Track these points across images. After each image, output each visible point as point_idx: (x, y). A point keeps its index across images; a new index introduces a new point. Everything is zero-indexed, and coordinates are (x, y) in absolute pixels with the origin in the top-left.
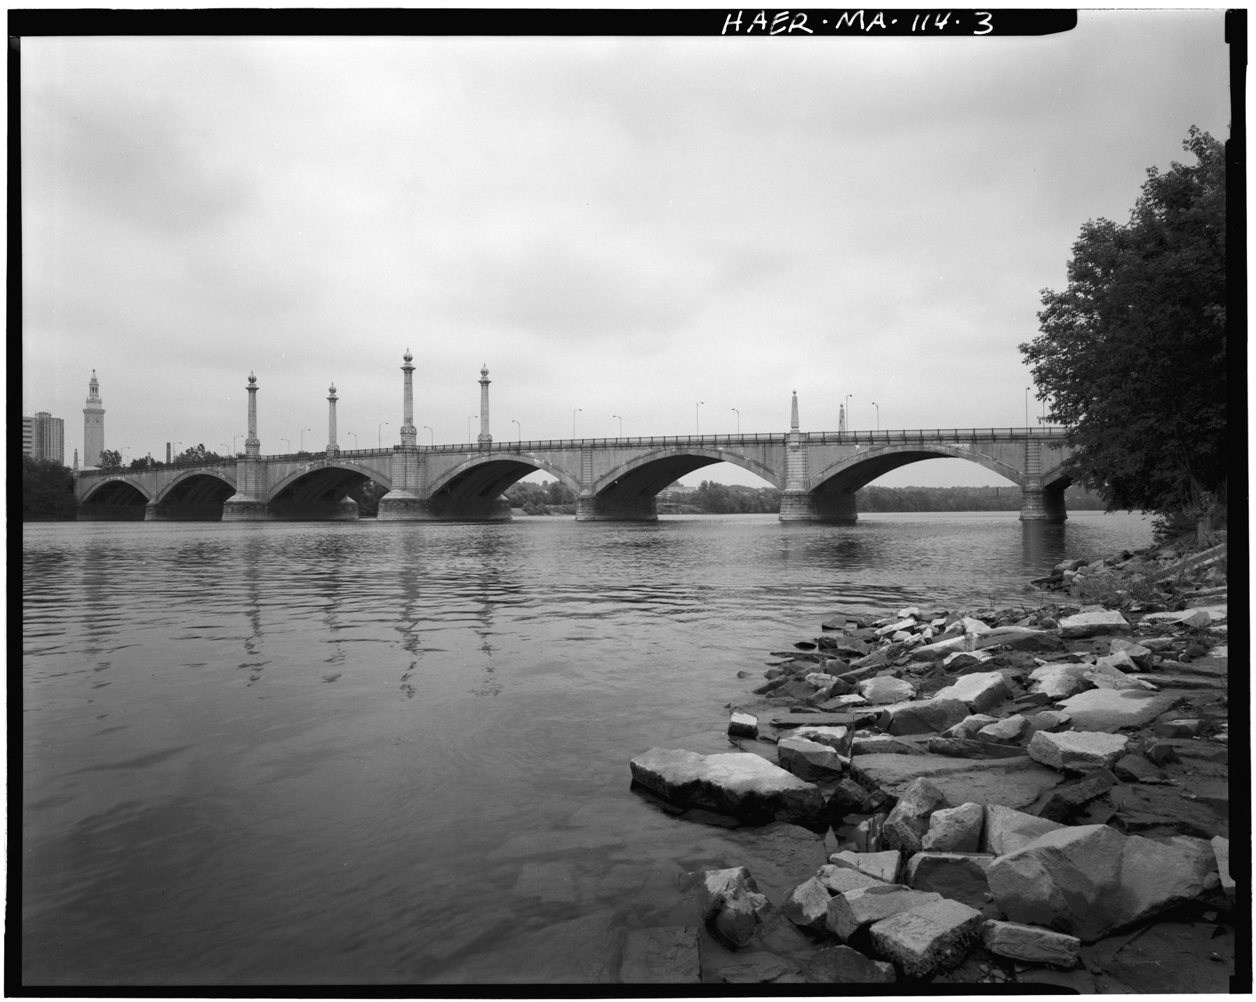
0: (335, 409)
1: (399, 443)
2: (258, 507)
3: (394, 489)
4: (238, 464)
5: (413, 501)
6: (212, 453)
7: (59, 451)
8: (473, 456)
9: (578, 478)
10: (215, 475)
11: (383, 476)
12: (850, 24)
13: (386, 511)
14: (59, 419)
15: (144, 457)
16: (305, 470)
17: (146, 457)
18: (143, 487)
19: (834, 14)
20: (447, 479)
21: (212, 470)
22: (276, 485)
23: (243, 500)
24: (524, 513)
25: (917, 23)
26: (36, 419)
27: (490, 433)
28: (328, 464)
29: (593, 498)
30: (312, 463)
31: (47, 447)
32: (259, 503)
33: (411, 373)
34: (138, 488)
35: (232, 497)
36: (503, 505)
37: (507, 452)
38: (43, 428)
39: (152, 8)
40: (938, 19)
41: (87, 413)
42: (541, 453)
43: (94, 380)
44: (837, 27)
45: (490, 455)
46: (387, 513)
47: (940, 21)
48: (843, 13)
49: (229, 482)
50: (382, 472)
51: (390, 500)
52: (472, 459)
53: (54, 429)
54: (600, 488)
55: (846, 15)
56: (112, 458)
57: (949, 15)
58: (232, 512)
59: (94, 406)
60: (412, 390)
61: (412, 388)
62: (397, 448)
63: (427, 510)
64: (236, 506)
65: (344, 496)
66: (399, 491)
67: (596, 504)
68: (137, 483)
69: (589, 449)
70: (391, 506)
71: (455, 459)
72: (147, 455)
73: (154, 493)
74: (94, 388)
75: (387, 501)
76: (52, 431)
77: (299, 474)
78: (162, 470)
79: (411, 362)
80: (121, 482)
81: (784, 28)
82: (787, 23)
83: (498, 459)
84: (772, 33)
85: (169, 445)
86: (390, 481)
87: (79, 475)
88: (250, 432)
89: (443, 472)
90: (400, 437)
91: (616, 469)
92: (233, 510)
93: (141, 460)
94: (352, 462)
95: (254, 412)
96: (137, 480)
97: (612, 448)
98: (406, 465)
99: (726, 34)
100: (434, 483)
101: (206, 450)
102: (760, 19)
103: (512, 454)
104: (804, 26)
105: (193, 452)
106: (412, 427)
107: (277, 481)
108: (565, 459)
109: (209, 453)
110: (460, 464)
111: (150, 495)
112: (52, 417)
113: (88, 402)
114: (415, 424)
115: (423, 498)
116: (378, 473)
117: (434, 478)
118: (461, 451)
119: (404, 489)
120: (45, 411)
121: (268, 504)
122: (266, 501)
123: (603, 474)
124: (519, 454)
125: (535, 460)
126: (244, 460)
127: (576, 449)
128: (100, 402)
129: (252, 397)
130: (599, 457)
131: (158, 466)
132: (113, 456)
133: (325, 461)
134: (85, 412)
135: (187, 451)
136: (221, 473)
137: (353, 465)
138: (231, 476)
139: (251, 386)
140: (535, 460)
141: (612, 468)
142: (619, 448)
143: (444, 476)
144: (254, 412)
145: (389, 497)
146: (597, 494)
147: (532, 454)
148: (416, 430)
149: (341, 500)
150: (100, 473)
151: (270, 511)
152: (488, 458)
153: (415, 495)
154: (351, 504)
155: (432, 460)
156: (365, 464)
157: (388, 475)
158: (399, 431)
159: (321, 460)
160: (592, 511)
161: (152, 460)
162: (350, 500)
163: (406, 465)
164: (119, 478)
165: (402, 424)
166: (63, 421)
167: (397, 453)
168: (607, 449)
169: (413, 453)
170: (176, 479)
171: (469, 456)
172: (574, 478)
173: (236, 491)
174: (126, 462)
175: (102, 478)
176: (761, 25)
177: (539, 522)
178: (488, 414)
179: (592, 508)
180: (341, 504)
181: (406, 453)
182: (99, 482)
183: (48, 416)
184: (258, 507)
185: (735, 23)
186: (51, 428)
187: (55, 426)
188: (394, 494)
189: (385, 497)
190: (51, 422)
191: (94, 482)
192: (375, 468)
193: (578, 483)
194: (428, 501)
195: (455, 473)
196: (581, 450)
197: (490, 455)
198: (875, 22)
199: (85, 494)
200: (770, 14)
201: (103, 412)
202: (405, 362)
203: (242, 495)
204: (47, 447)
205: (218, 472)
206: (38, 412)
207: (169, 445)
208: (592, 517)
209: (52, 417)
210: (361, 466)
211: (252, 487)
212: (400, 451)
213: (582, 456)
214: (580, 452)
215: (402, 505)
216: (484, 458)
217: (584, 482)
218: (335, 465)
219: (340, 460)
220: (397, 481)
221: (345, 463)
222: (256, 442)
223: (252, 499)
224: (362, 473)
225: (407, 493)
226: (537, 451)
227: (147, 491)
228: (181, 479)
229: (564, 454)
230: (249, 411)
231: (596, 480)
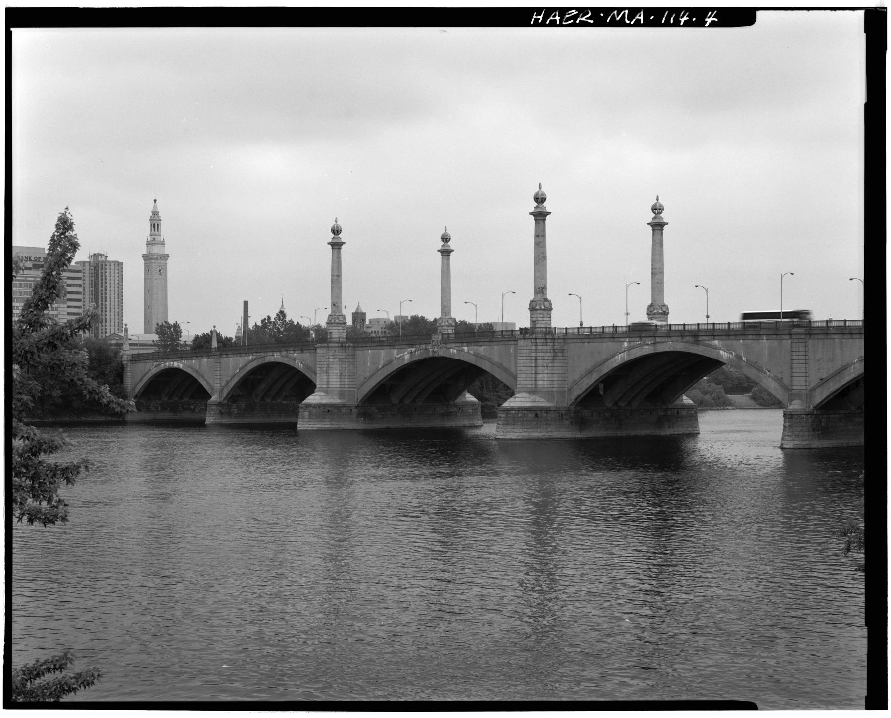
0: (448, 265)
2: (344, 410)
3: (519, 392)
4: (318, 351)
5: (547, 410)
7: (117, 307)
8: (632, 344)
9: (786, 381)
10: (291, 364)
11: (506, 370)
12: (618, 19)
14: (117, 262)
15: (209, 332)
17: (211, 332)
18: (203, 377)
19: (608, 11)
21: (287, 357)
22: (367, 380)
23: (324, 401)
26: (89, 262)
27: (666, 302)
28: (433, 351)
30: (413, 350)
31: (102, 301)
32: (344, 406)
33: (544, 220)
34: (198, 379)
35: (311, 397)
37: (679, 339)
38: (97, 275)
39: (108, 7)
40: (581, 16)
41: (148, 260)
42: (729, 342)
43: (155, 214)
44: (608, 21)
45: (655, 343)
46: (509, 428)
47: (682, 17)
49: (309, 375)
50: (505, 365)
51: (512, 408)
52: (629, 349)
53: (110, 275)
54: (820, 396)
55: (615, 12)
56: (171, 332)
59: (156, 250)
60: (545, 246)
62: (523, 331)
63: (567, 422)
64: (314, 410)
65: (460, 392)
66: (527, 395)
68: (197, 372)
71: (607, 347)
72: (213, 329)
73: (217, 386)
74: (155, 225)
75: (508, 410)
76: (108, 278)
77: (396, 366)
78: (227, 354)
79: (544, 204)
80: (177, 371)
81: (572, 21)
82: (575, 17)
83: (667, 349)
85: (246, 303)
87: (130, 358)
88: (334, 305)
90: (529, 315)
91: (844, 369)
92: (311, 414)
93: (204, 335)
94: (466, 348)
95: (339, 276)
96: (197, 368)
97: (836, 336)
98: (536, 357)
100: (576, 383)
101: (288, 319)
102: (640, 16)
104: (539, 19)
105: (271, 323)
106: (546, 300)
107: (368, 374)
108: (766, 352)
109: (291, 322)
110: (613, 356)
111: (212, 389)
112: (109, 259)
113: (149, 244)
115: (560, 405)
117: (576, 376)
118: (613, 335)
119: (533, 391)
120: (100, 252)
121: (357, 407)
123: (824, 376)
124: (697, 342)
125: (722, 352)
126: (326, 345)
127: (783, 336)
128: (163, 243)
129: (335, 255)
130: (818, 348)
131: (226, 346)
132: (172, 329)
134: (161, 220)
135: (262, 321)
136: (297, 360)
137: (465, 352)
140: (722, 352)
141: (838, 365)
142: (849, 336)
143: (590, 372)
144: (338, 276)
145: (512, 404)
147: (716, 342)
148: (551, 304)
149: (456, 398)
150: (155, 357)
153: (548, 401)
154: (472, 404)
156: (483, 353)
157: (513, 370)
159: (424, 346)
161: (219, 335)
162: (470, 397)
163: (536, 357)
164: (176, 365)
165: (532, 297)
166: (122, 264)
167: (524, 339)
168: (829, 337)
169: (546, 339)
170: (243, 368)
171: (626, 344)
172: (779, 380)
173: (315, 386)
174: (189, 334)
175: (155, 364)
181: (536, 339)
182: (152, 369)
183: (104, 258)
185: (555, 18)
186: (108, 274)
187: (113, 272)
188: (518, 401)
190: (108, 267)
191: (147, 369)
192: (496, 358)
195: (606, 369)
197: (655, 343)
198: (637, 17)
199: (137, 384)
200: (563, 11)
201: (167, 256)
203: (322, 393)
204: (102, 301)
205: (295, 359)
206: (92, 254)
207: (246, 303)
208: (806, 442)
209: (109, 259)
210: (476, 355)
211: (335, 382)
212: (527, 336)
214: (789, 341)
215: (530, 415)
216: (647, 347)
217: (795, 388)
218: (441, 353)
219: (449, 345)
220: (523, 380)
223: (336, 400)
224: (478, 365)
225: (537, 399)
226: (723, 337)
227: (208, 383)
228: (249, 368)
230: (333, 276)
231: (812, 386)
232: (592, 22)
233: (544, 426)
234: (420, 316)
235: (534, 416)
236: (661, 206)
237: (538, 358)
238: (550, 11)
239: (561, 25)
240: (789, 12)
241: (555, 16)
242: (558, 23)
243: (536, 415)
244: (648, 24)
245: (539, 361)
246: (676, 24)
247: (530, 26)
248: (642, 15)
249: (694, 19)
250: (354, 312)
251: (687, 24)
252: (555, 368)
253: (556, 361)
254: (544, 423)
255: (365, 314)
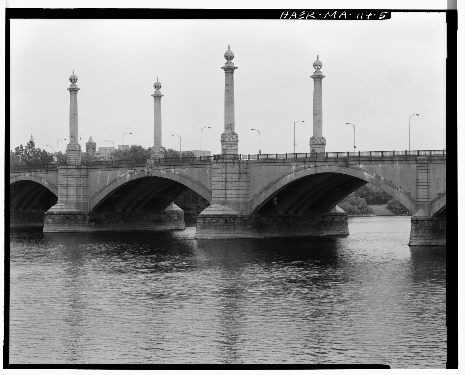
1: (220, 152)
2: (79, 217)
3: (213, 203)
4: (60, 171)
5: (234, 217)
6: (42, 151)
8: (298, 167)
9: (413, 195)
10: (38, 181)
11: (204, 187)
13: (205, 228)
16: (125, 179)
20: (270, 192)
22: (97, 194)
23: (64, 210)
24: (388, 211)
25: (113, 231)
27: (324, 135)
28: (148, 172)
29: (430, 220)
30: (133, 171)
32: (79, 214)
33: (232, 73)
35: (53, 207)
36: (337, 219)
37: (334, 163)
42: (371, 166)
45: (316, 166)
46: (206, 231)
48: (328, 12)
49: (52, 190)
51: (208, 216)
52: (296, 171)
57: (288, 12)
58: (53, 223)
61: (233, 89)
62: (216, 157)
63: (249, 226)
64: (56, 217)
65: (168, 204)
66: (219, 205)
67: (433, 226)
69: (426, 162)
70: (209, 223)
71: (280, 169)
75: (205, 217)
77: (120, 183)
83: (325, 171)
84: (299, 19)
86: (210, 192)
88: (71, 136)
89: (266, 184)
94: (173, 170)
98: (226, 176)
99: (362, 19)
100: (256, 196)
103: (339, 166)
106: (234, 133)
107: (98, 190)
109: (39, 150)
110: (284, 177)
114: (236, 130)
115: (244, 213)
116: (199, 183)
117: (257, 192)
119: (224, 203)
121: (89, 215)
122: (86, 211)
124: (347, 166)
126: (65, 167)
127: (411, 162)
133: (145, 169)
135: (16, 149)
138: (53, 183)
139: (72, 87)
140: (365, 173)
143: (267, 188)
146: (434, 215)
147: (361, 166)
148: (237, 137)
149: (165, 208)
151: (91, 221)
152: (313, 170)
153: (235, 210)
154: (177, 212)
155: (254, 170)
156: (185, 174)
157: (208, 187)
158: (220, 139)
159: (141, 168)
160: (429, 235)
162: (175, 207)
163: (226, 176)
167: (217, 163)
169: (234, 163)
171: (294, 167)
173: (57, 199)
176: (295, 16)
177: (133, 362)
178: (321, 114)
179: (427, 231)
180: (165, 213)
181: (226, 163)
184: (79, 217)
185: (294, 15)
189: (203, 213)
192: (196, 178)
193: (413, 201)
194: (250, 217)
196: (416, 163)
197: (316, 166)
202: (226, 61)
210: (181, 175)
212: (219, 161)
213: (417, 170)
214: (415, 165)
215: (221, 221)
216: (309, 169)
217: (420, 200)
218: (155, 173)
220: (217, 194)
221: (165, 172)
222: (77, 147)
223: (73, 210)
225: (227, 208)
229: (397, 166)
230: (71, 114)
231: (432, 199)
232: (314, 17)
233: (232, 229)
234: (138, 145)
235: (224, 221)
236: (320, 63)
237: (228, 178)
238: (291, 11)
239: (297, 18)
240: (426, 13)
241: (294, 14)
242: (296, 17)
243: (226, 221)
244: (349, 18)
245: (228, 180)
246: (365, 18)
247: (356, 19)
248: (295, 14)
249: (375, 15)
250: (87, 142)
251: (371, 18)
252: (241, 185)
253: (241, 180)
254: (232, 227)
255: (95, 143)
